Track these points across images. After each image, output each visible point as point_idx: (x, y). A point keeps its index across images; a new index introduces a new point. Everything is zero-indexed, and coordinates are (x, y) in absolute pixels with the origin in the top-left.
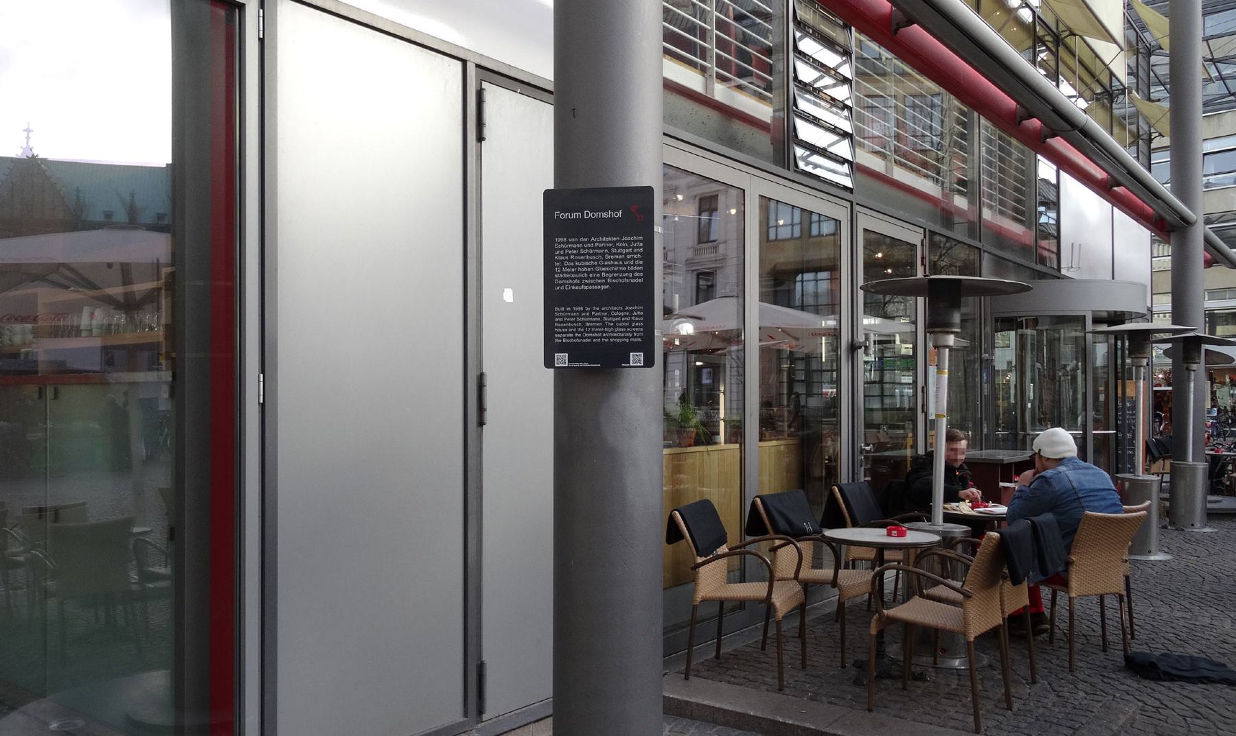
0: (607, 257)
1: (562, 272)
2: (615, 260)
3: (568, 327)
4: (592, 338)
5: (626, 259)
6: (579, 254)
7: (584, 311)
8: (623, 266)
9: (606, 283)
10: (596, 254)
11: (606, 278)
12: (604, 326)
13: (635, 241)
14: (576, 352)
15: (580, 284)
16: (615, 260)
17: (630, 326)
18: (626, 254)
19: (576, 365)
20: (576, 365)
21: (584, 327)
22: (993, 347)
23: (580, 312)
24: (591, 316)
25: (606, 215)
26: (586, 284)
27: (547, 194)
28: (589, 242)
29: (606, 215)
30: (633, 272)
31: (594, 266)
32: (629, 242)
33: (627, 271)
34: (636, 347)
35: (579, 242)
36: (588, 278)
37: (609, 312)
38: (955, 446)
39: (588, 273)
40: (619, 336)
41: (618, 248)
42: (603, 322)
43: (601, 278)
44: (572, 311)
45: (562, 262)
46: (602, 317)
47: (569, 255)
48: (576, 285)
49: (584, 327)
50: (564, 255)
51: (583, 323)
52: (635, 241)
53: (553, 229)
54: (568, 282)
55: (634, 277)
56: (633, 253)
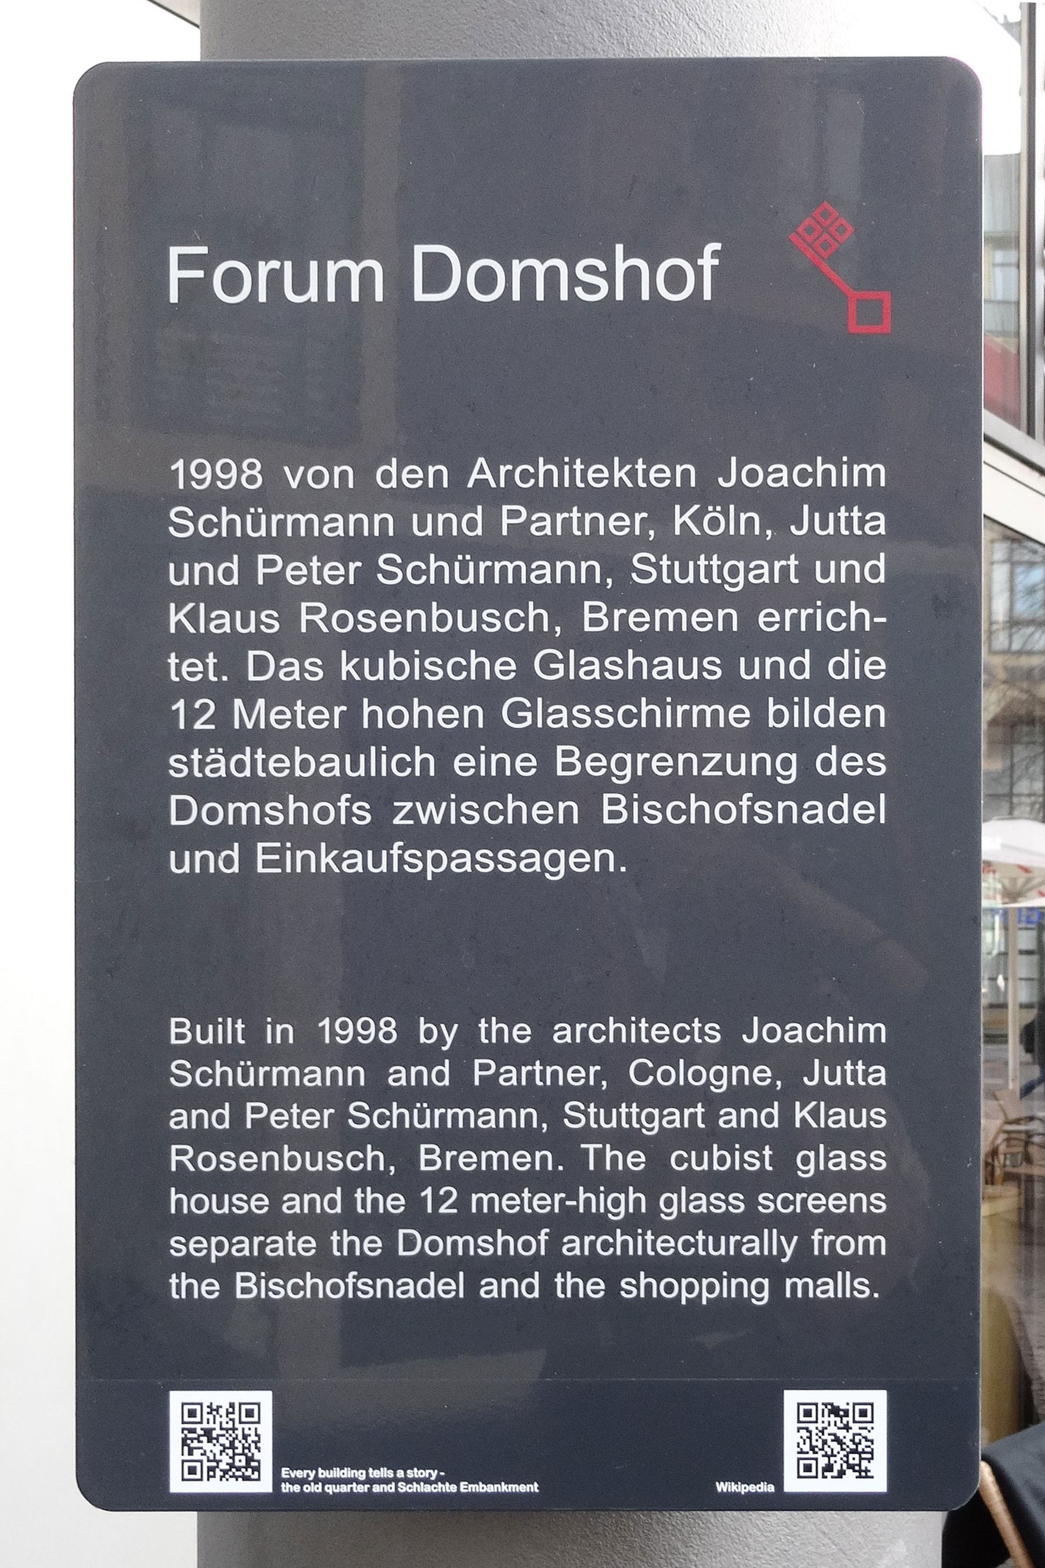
0: (595, 617)
1: (231, 739)
2: (651, 644)
3: (273, 1183)
4: (477, 1269)
5: (750, 641)
6: (367, 593)
7: (409, 1051)
8: (728, 690)
9: (589, 833)
10: (514, 595)
11: (589, 790)
12: (571, 1174)
13: (827, 499)
14: (348, 1382)
15: (376, 837)
16: (651, 644)
17: (783, 1178)
18: (752, 599)
19: (347, 1480)
20: (347, 1480)
21: (409, 1180)
22: (1031, 1348)
23: (376, 1057)
24: (462, 1092)
25: (594, 280)
26: (421, 837)
27: (117, 106)
28: (458, 497)
29: (594, 280)
30: (807, 742)
31: (489, 693)
32: (778, 507)
33: (760, 737)
34: (833, 1350)
35: (365, 497)
36: (439, 786)
37: (613, 1058)
38: (1013, 693)
39: (444, 744)
40: (681, 1253)
41: (686, 548)
42: (565, 1144)
43: (545, 786)
44: (310, 1050)
45: (229, 650)
46: (550, 1100)
47: (278, 595)
48: (345, 837)
49: (409, 1180)
50: (246, 597)
51: (400, 1144)
52: (827, 499)
53: (145, 382)
54: (279, 811)
55: (810, 786)
56: (807, 592)
